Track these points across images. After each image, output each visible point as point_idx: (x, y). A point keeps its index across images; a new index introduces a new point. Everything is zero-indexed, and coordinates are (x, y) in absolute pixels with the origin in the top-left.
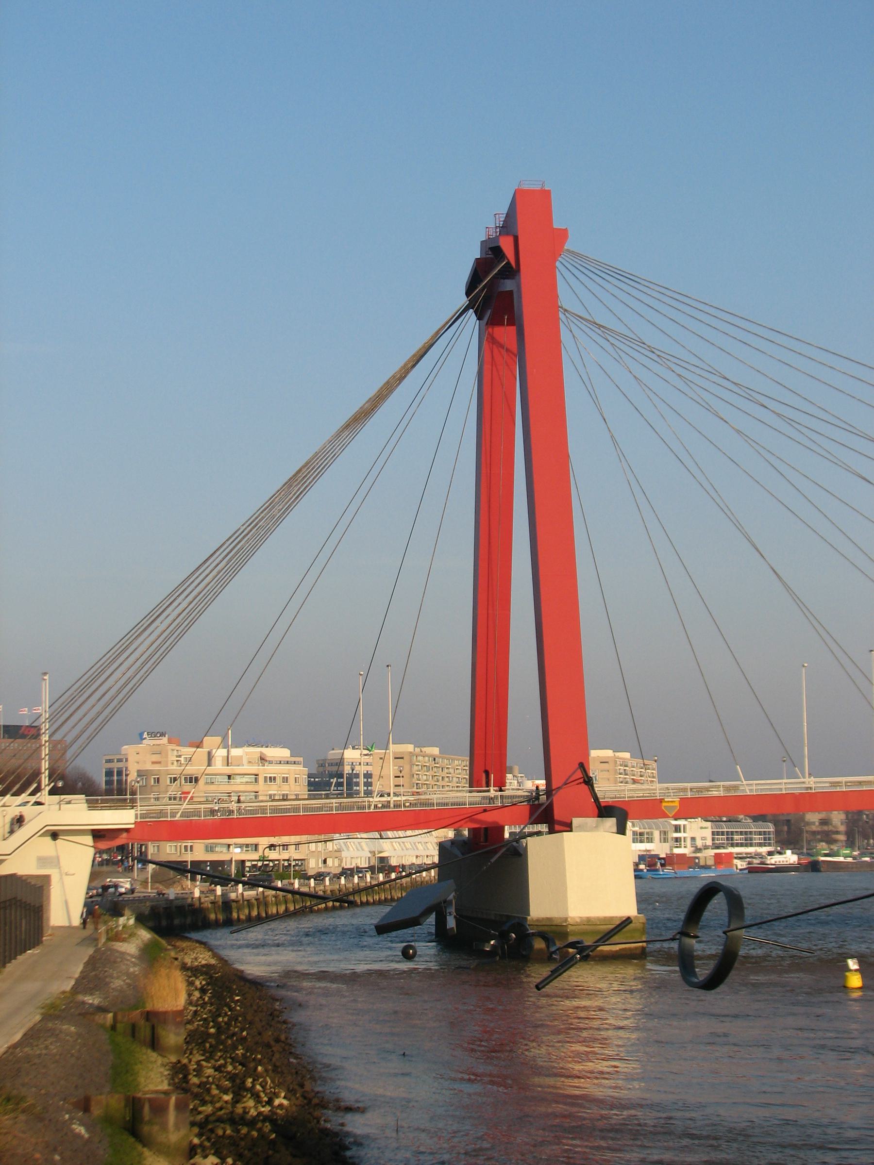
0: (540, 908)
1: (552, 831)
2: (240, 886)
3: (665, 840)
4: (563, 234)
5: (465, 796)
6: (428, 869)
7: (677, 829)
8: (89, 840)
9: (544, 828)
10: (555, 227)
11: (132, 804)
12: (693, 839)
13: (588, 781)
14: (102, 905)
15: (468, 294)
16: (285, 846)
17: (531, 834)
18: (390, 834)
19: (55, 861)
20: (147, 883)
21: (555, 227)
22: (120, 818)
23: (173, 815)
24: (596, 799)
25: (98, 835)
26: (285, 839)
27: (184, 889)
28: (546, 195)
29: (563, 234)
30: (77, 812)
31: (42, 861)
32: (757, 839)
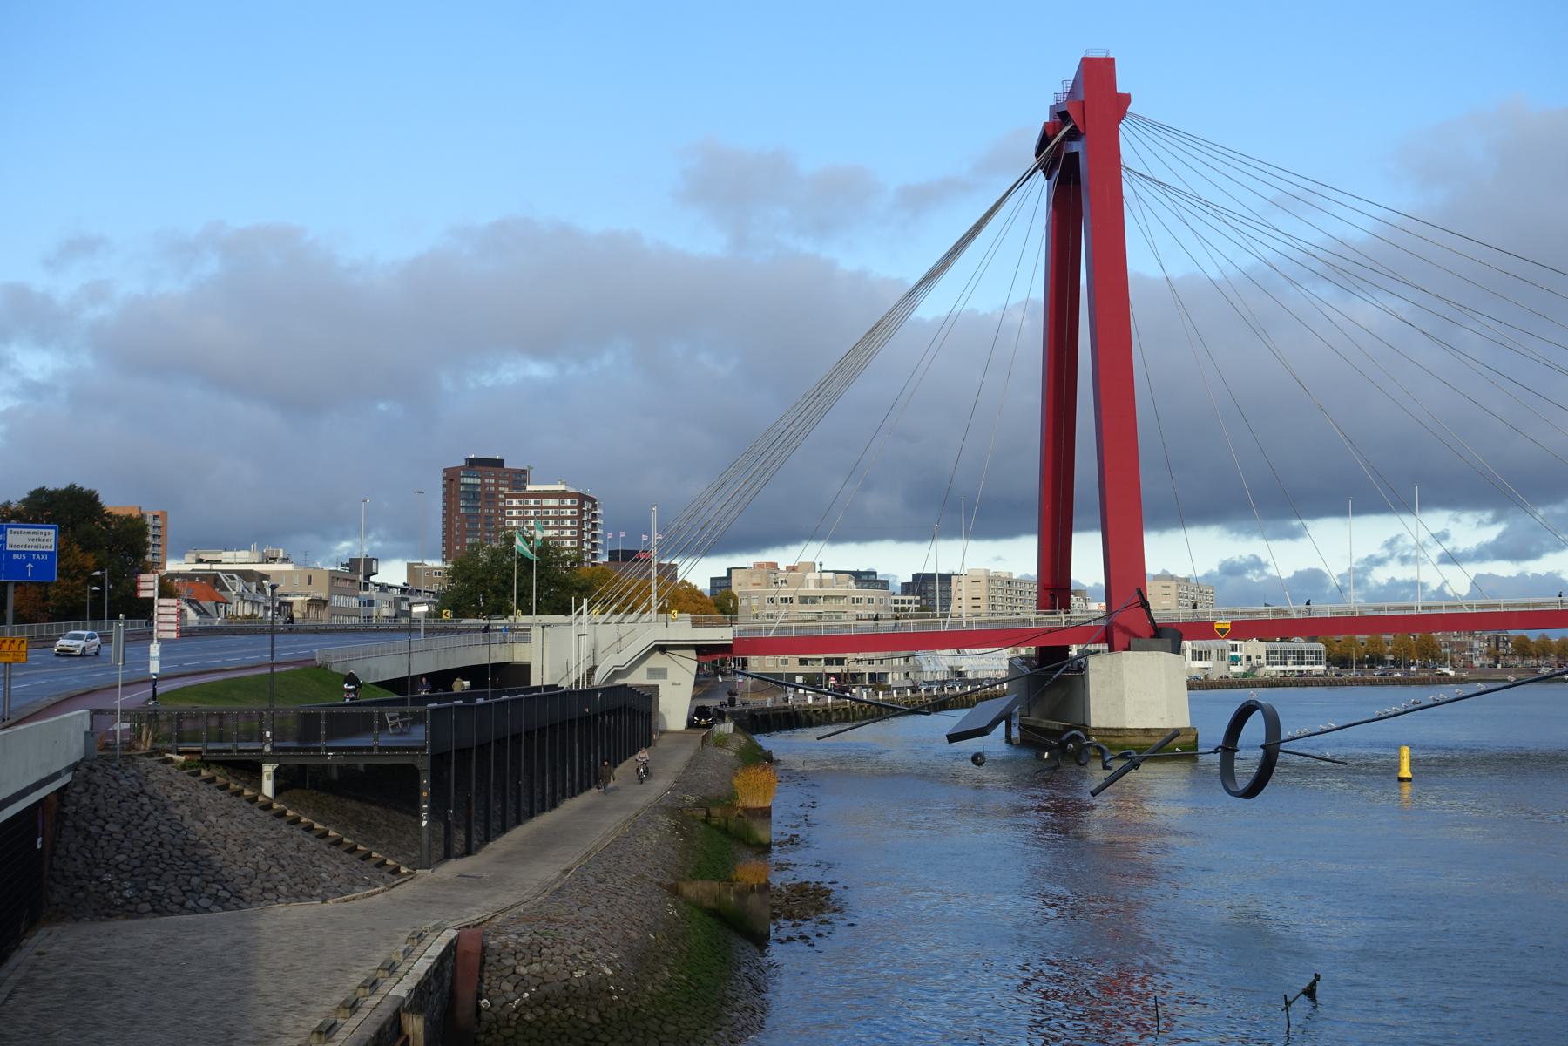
0: (1099, 717)
1: (1111, 650)
2: (66, 810)
3: (1223, 659)
4: (1126, 99)
5: (1030, 614)
6: (1001, 682)
7: (1234, 648)
8: (692, 654)
9: (1106, 647)
10: (1095, 722)
11: (733, 622)
12: (1249, 658)
13: (1145, 605)
14: (701, 717)
15: (1037, 155)
16: (871, 662)
17: (1091, 653)
18: (967, 651)
19: (662, 673)
20: (220, 741)
21: (1095, 722)
22: (721, 634)
23: (768, 629)
24: (1153, 620)
25: (702, 650)
26: (871, 655)
27: (424, 749)
28: (1110, 62)
29: (1126, 99)
30: (681, 629)
31: (652, 672)
32: (1308, 658)
